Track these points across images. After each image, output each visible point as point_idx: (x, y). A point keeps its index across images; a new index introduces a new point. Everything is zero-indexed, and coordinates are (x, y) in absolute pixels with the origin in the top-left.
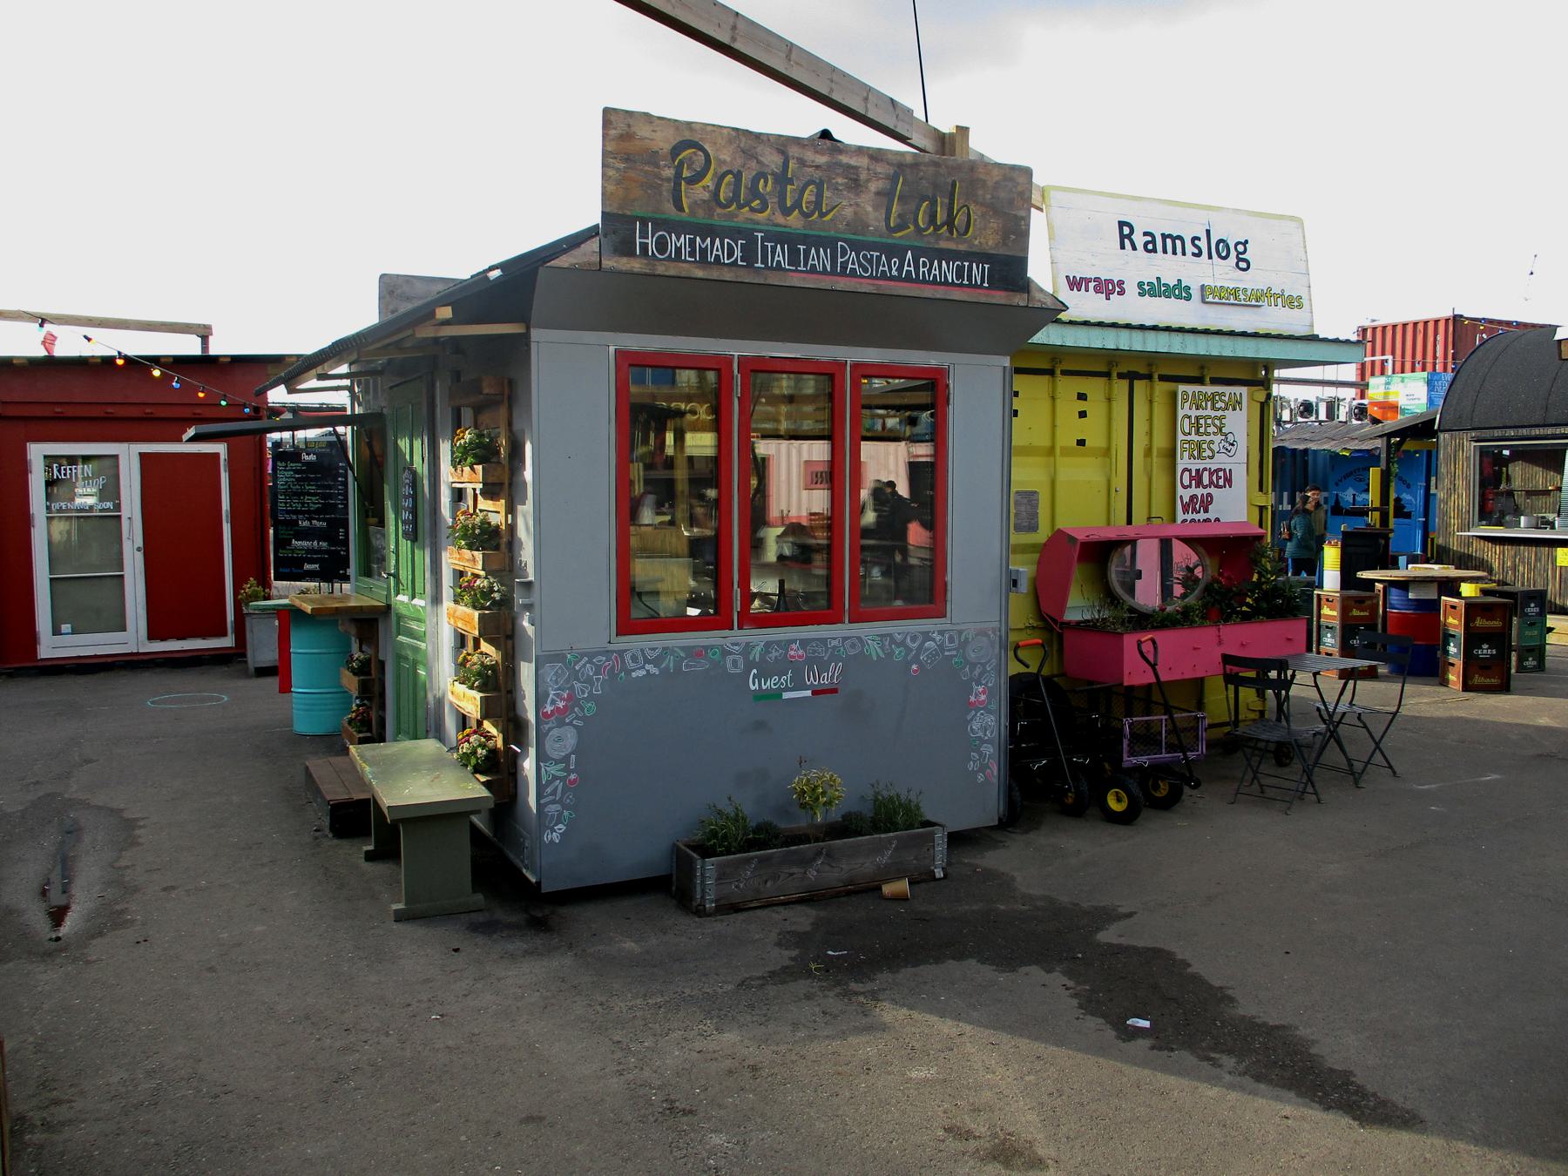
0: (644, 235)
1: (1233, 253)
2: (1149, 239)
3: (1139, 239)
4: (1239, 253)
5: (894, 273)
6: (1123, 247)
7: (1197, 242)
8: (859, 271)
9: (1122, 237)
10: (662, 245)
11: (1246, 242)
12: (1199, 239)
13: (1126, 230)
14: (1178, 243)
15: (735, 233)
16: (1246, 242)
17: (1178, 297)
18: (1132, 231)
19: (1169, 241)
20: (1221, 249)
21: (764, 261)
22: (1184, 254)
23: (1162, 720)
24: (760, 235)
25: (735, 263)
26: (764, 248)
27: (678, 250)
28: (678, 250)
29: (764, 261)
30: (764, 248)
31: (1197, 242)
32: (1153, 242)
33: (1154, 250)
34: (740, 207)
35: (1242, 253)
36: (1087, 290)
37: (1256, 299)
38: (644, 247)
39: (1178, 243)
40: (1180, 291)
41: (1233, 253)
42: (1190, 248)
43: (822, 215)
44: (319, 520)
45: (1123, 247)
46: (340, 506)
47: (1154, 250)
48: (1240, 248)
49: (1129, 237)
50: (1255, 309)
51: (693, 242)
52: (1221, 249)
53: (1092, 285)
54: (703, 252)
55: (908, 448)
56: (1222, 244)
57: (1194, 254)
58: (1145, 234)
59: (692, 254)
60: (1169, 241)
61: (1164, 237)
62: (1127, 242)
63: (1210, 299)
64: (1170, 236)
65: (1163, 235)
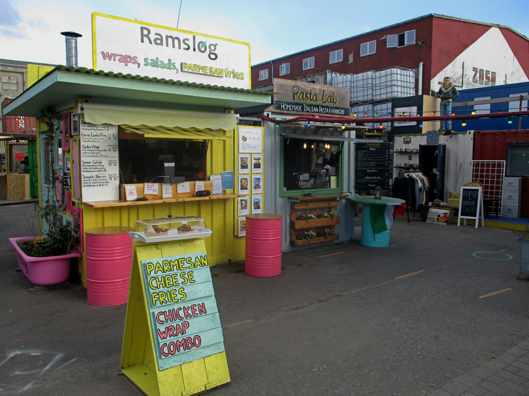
0: (283, 105)
1: (208, 50)
2: (159, 37)
3: (152, 37)
4: (211, 50)
5: (330, 112)
6: (142, 41)
7: (186, 42)
8: (323, 112)
9: (143, 35)
10: (285, 107)
11: (217, 45)
12: (188, 40)
13: (145, 32)
14: (176, 41)
15: (300, 104)
16: (217, 45)
17: (168, 68)
18: (149, 32)
19: (170, 40)
20: (201, 47)
21: (305, 110)
22: (180, 48)
23: (475, 216)
24: (305, 105)
25: (300, 111)
26: (305, 107)
27: (288, 108)
28: (288, 108)
29: (305, 110)
30: (305, 107)
31: (186, 42)
32: (161, 40)
33: (161, 44)
34: (304, 100)
35: (213, 50)
36: (115, 60)
37: (218, 74)
38: (283, 107)
39: (176, 41)
40: (170, 65)
41: (208, 50)
42: (183, 46)
43: (317, 101)
44: (375, 170)
45: (142, 41)
46: (386, 165)
47: (161, 44)
48: (212, 48)
49: (147, 36)
50: (221, 78)
51: (291, 107)
52: (201, 47)
53: (117, 58)
54: (294, 108)
55: (416, 153)
56: (201, 44)
57: (184, 49)
58: (156, 34)
59: (291, 109)
60: (170, 40)
61: (167, 37)
62: (145, 39)
63: (186, 70)
64: (171, 37)
65: (167, 36)
